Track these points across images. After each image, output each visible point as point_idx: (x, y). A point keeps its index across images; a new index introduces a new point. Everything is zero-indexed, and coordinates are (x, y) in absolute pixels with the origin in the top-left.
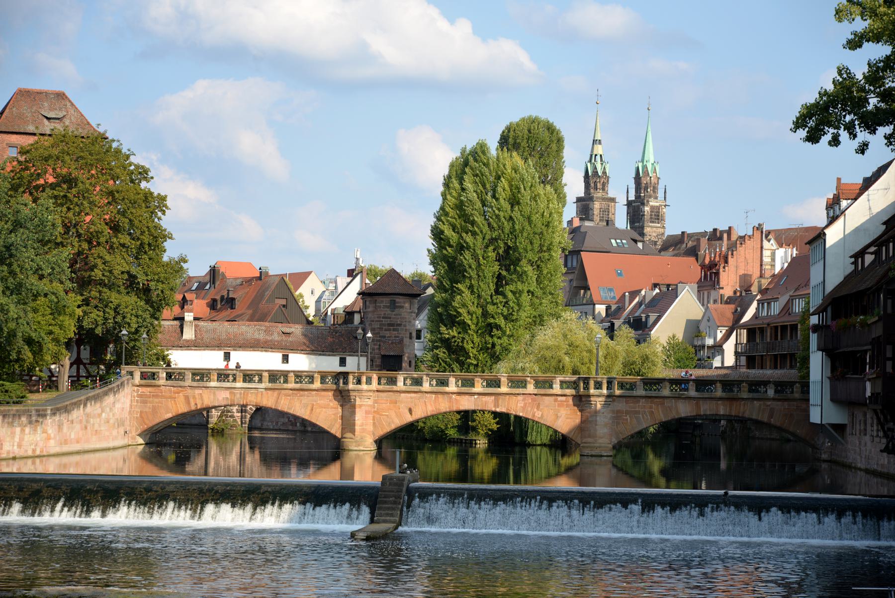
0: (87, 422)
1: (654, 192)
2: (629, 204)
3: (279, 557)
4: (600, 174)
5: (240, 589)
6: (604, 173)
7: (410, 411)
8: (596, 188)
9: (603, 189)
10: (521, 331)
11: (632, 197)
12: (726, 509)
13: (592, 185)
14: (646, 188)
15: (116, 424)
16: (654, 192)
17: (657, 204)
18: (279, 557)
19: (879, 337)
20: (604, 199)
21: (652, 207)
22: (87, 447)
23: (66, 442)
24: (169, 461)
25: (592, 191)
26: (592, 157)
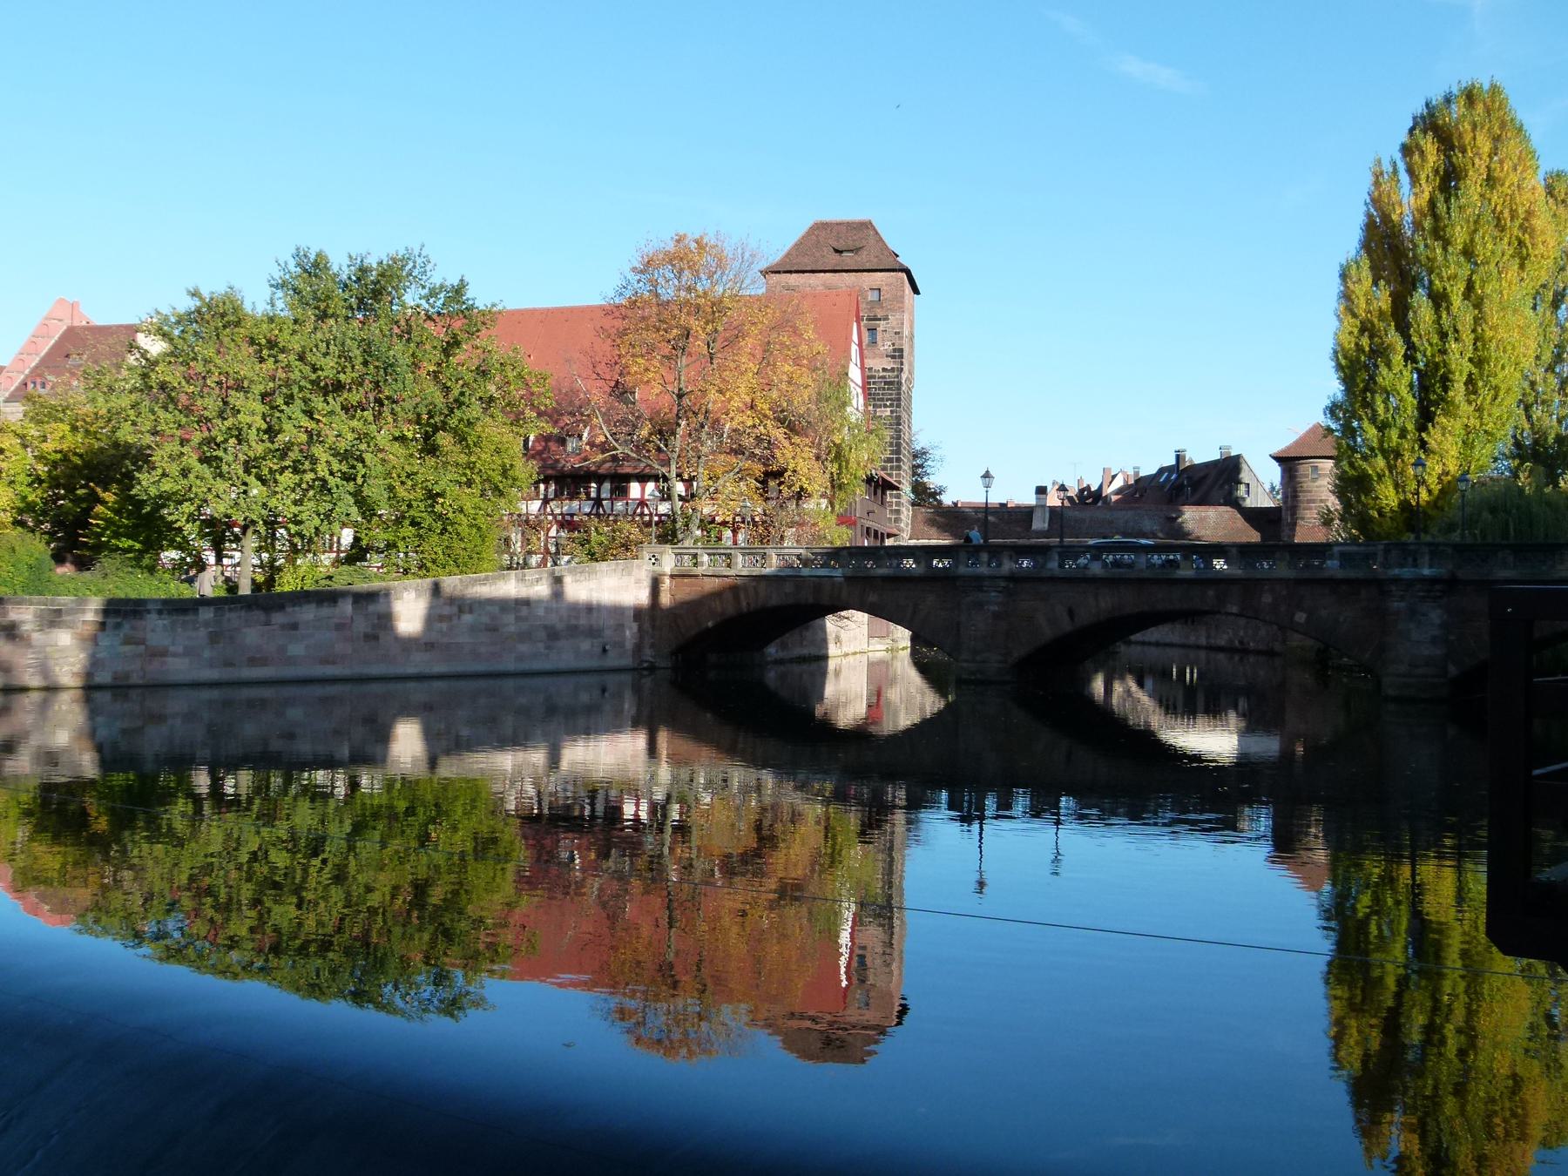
7: (1071, 613)
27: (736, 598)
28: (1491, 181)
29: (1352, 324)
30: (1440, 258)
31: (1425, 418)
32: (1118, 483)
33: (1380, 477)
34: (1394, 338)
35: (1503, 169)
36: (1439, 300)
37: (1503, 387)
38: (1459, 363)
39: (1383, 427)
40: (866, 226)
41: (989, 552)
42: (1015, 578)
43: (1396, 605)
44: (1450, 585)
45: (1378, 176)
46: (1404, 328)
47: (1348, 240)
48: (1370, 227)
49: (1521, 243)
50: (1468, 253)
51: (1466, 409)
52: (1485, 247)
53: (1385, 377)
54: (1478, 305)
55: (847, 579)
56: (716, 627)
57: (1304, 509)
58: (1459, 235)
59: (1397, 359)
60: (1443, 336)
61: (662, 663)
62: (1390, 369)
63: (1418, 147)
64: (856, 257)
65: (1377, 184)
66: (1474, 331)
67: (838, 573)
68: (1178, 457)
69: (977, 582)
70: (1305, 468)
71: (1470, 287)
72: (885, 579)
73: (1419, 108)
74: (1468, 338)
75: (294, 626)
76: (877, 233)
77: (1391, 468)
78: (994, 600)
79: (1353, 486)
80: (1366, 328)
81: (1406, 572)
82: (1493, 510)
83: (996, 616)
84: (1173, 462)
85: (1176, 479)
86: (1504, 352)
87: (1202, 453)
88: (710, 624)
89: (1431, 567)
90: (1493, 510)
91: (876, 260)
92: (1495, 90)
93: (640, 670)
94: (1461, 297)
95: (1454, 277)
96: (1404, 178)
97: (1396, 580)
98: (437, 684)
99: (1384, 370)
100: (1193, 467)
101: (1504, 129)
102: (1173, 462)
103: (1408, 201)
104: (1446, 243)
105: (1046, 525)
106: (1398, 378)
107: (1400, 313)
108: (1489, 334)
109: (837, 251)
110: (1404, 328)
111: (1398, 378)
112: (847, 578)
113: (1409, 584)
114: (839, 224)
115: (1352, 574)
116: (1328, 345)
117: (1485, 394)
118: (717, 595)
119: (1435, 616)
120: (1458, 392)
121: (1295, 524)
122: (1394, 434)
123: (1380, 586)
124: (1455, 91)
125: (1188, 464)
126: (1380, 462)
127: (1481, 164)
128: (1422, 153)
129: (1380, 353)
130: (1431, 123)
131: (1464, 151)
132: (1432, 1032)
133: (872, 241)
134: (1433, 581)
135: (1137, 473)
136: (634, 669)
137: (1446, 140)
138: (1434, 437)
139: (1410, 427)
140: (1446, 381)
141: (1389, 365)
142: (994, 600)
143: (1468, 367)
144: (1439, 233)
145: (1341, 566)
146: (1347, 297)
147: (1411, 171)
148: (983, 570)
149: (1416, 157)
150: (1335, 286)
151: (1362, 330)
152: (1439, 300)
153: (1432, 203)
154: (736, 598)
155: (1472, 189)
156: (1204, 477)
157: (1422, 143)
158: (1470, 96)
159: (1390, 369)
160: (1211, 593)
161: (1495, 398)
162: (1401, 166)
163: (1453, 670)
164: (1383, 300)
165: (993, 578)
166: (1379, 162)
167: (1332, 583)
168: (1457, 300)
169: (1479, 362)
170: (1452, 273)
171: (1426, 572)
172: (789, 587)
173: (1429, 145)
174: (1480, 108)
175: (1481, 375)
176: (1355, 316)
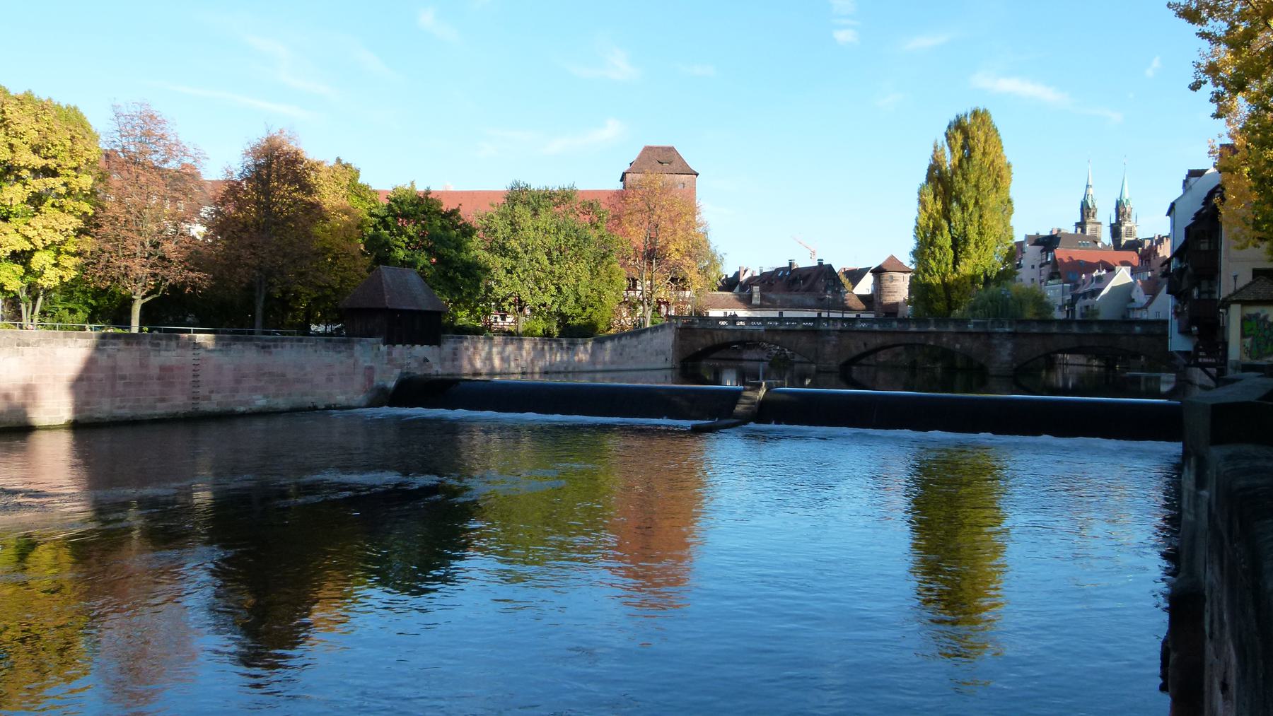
0: (622, 350)
1: (1129, 217)
2: (1112, 225)
3: (116, 605)
4: (1091, 207)
5: (99, 652)
6: (1094, 206)
7: (865, 344)
8: (1088, 216)
9: (1093, 216)
10: (1236, 35)
11: (1114, 221)
12: (174, 275)
13: (1086, 214)
14: (1123, 215)
15: (655, 353)
16: (1129, 217)
17: (1131, 225)
18: (116, 605)
19: (1175, 307)
20: (1093, 223)
21: (1127, 228)
24: (856, 326)
25: (1085, 218)
26: (1086, 195)
28: (984, 154)
30: (964, 188)
32: (748, 275)
34: (944, 223)
35: (990, 149)
36: (964, 207)
37: (989, 245)
38: (973, 236)
40: (671, 149)
41: (898, 321)
42: (841, 331)
43: (995, 342)
45: (936, 147)
48: (931, 169)
49: (996, 181)
50: (977, 186)
51: (975, 255)
53: (940, 240)
55: (766, 330)
57: (887, 296)
58: (973, 178)
59: (946, 232)
61: (375, 384)
62: (942, 237)
64: (670, 166)
65: (935, 151)
66: (979, 221)
67: (763, 328)
68: (790, 264)
69: (828, 332)
71: (977, 203)
72: (783, 330)
73: (953, 118)
76: (678, 154)
78: (833, 339)
81: (1000, 330)
83: (834, 346)
84: (788, 265)
85: (789, 275)
86: (991, 230)
88: (700, 349)
89: (1009, 328)
91: (681, 168)
92: (985, 112)
93: (673, 368)
94: (973, 206)
95: (970, 197)
96: (947, 149)
98: (634, 373)
99: (940, 238)
101: (991, 132)
102: (788, 265)
103: (949, 161)
105: (759, 302)
107: (946, 214)
108: (985, 222)
109: (660, 162)
111: (945, 240)
113: (1001, 334)
114: (658, 148)
115: (978, 330)
119: (1009, 345)
120: (971, 247)
123: (989, 335)
125: (795, 267)
127: (981, 146)
128: (955, 139)
129: (937, 228)
131: (973, 140)
133: (677, 158)
134: (1009, 333)
135: (761, 271)
136: (672, 368)
140: (966, 241)
142: (833, 339)
143: (976, 236)
145: (974, 327)
147: (950, 145)
148: (831, 327)
152: (964, 207)
156: (809, 276)
157: (955, 134)
159: (942, 237)
160: (923, 337)
161: (985, 250)
162: (946, 143)
163: (1015, 365)
165: (834, 331)
166: (936, 141)
167: (970, 333)
169: (980, 234)
170: (969, 196)
171: (1007, 330)
172: (738, 334)
175: (981, 240)
176: (926, 211)
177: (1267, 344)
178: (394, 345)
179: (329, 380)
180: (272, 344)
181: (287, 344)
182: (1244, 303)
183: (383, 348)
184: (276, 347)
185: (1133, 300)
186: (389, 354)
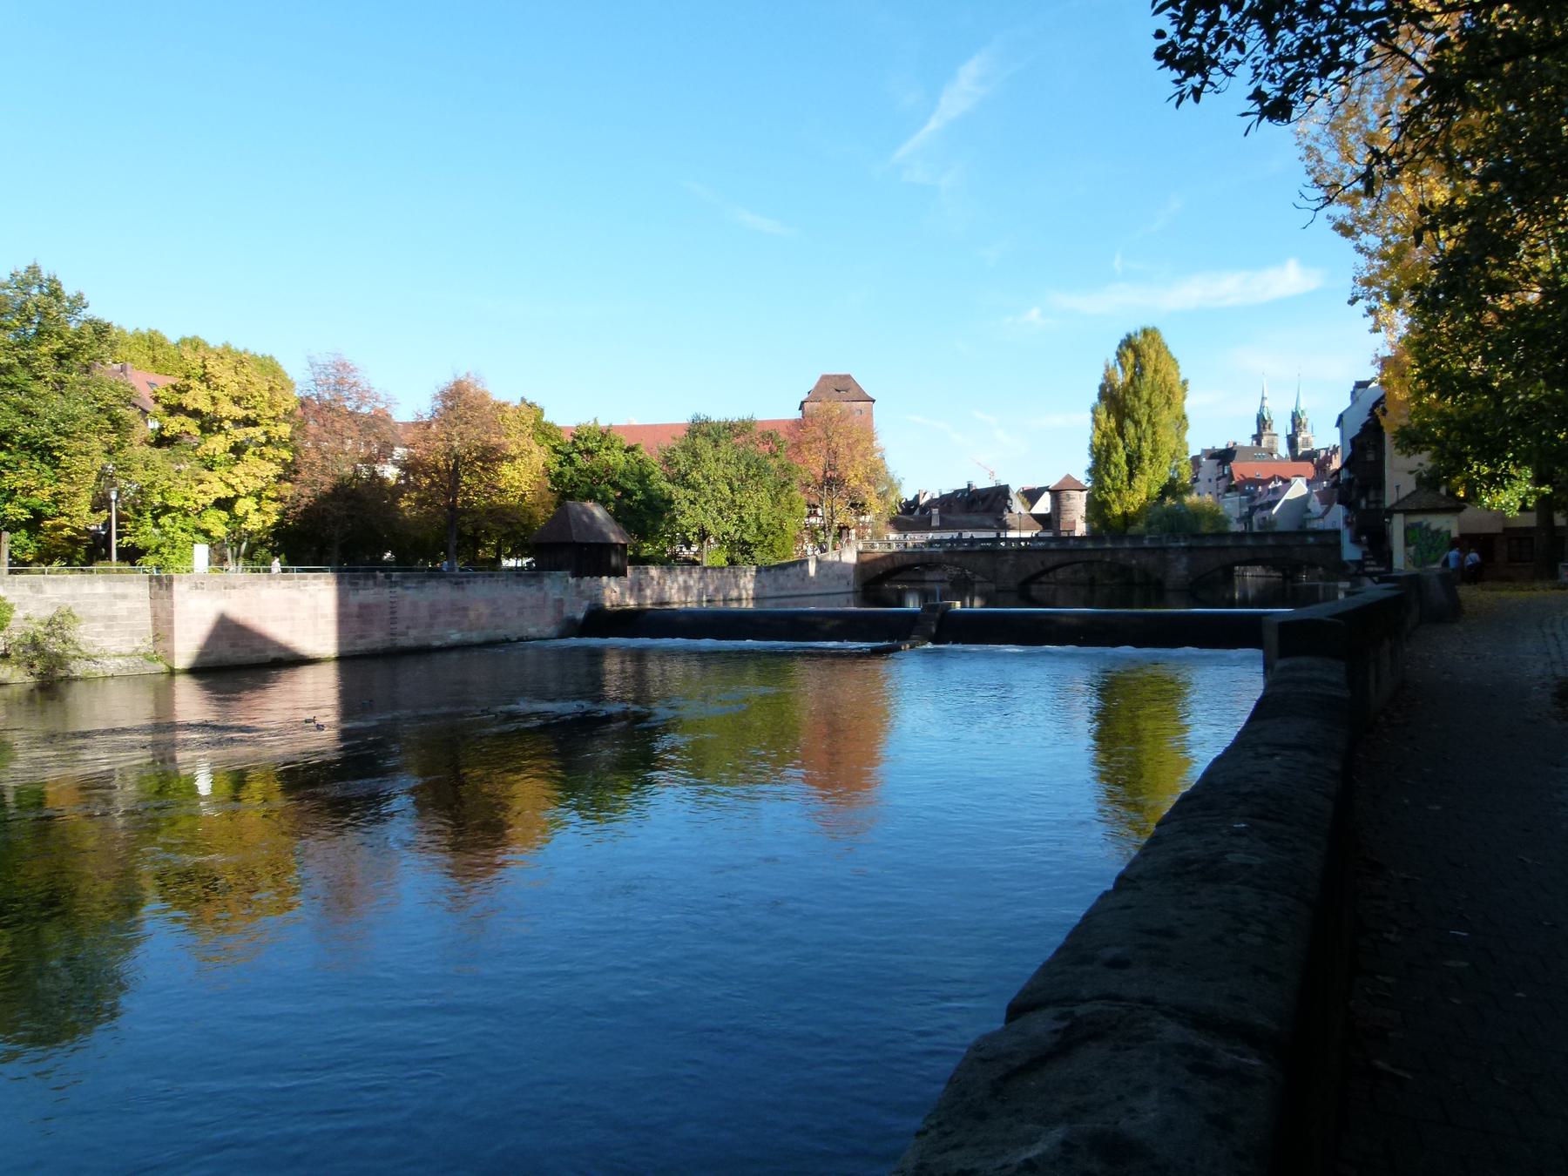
7: (1042, 563)
22: (804, 592)
23: (782, 589)
27: (893, 560)
28: (1156, 371)
29: (1098, 433)
31: (1131, 476)
32: (927, 498)
33: (1114, 501)
34: (1119, 440)
35: (1162, 366)
39: (1113, 480)
40: (848, 377)
44: (1189, 549)
45: (1107, 367)
46: (1122, 436)
47: (1093, 396)
48: (1102, 388)
50: (1149, 403)
51: (1150, 472)
52: (1156, 400)
54: (1153, 425)
56: (884, 574)
58: (1145, 395)
59: (1120, 449)
60: (1140, 439)
63: (1125, 355)
67: (941, 550)
70: (1063, 495)
71: (1150, 417)
73: (1123, 336)
74: (1150, 440)
75: (788, 576)
77: (1119, 497)
79: (1096, 508)
80: (1104, 435)
82: (1167, 516)
87: (983, 483)
90: (1167, 516)
93: (855, 592)
96: (1119, 368)
97: (1171, 548)
99: (1115, 455)
100: (977, 491)
104: (1140, 399)
106: (1120, 457)
110: (1122, 436)
111: (1120, 457)
112: (945, 552)
115: (1153, 545)
116: (1088, 443)
117: (1156, 465)
118: (883, 559)
119: (1184, 560)
121: (1059, 521)
122: (1119, 483)
123: (1165, 550)
124: (1139, 331)
126: (1113, 495)
130: (1128, 343)
132: (740, 991)
134: (1184, 547)
137: (1138, 353)
138: (1136, 483)
139: (1125, 479)
140: (1140, 458)
141: (1117, 453)
143: (1150, 453)
144: (1137, 394)
146: (1096, 421)
149: (1124, 360)
150: (1090, 415)
151: (1103, 437)
152: (1137, 423)
153: (1132, 380)
154: (893, 560)
155: (1149, 373)
156: (987, 496)
158: (1145, 332)
163: (1191, 579)
164: (1113, 424)
167: (1145, 549)
168: (1144, 425)
169: (1154, 451)
170: (1142, 413)
171: (1182, 544)
172: (917, 556)
173: (1130, 355)
174: (1150, 338)
177: (1430, 552)
178: (582, 577)
179: (520, 613)
180: (465, 580)
181: (480, 580)
182: (1407, 512)
183: (572, 581)
184: (468, 582)
185: (1309, 511)
186: (578, 586)
